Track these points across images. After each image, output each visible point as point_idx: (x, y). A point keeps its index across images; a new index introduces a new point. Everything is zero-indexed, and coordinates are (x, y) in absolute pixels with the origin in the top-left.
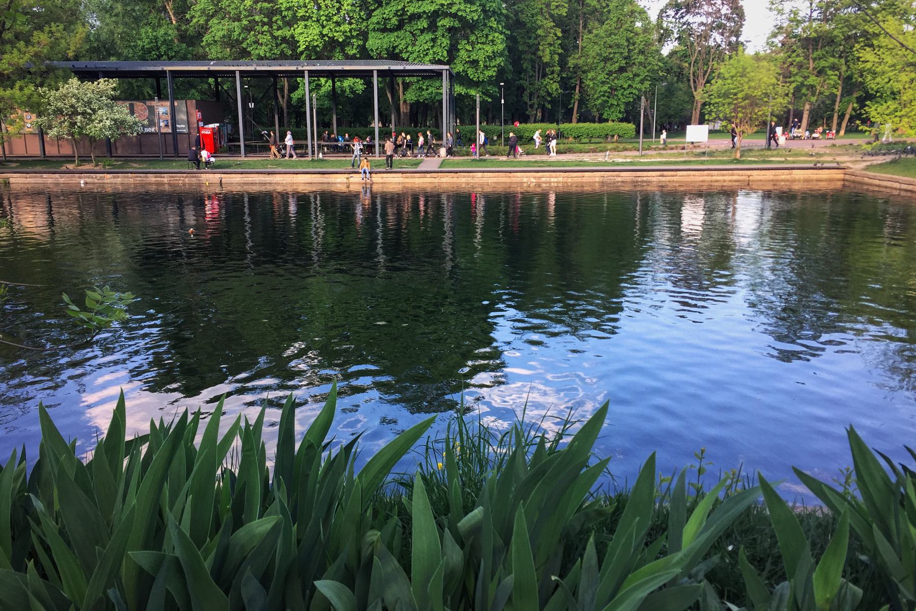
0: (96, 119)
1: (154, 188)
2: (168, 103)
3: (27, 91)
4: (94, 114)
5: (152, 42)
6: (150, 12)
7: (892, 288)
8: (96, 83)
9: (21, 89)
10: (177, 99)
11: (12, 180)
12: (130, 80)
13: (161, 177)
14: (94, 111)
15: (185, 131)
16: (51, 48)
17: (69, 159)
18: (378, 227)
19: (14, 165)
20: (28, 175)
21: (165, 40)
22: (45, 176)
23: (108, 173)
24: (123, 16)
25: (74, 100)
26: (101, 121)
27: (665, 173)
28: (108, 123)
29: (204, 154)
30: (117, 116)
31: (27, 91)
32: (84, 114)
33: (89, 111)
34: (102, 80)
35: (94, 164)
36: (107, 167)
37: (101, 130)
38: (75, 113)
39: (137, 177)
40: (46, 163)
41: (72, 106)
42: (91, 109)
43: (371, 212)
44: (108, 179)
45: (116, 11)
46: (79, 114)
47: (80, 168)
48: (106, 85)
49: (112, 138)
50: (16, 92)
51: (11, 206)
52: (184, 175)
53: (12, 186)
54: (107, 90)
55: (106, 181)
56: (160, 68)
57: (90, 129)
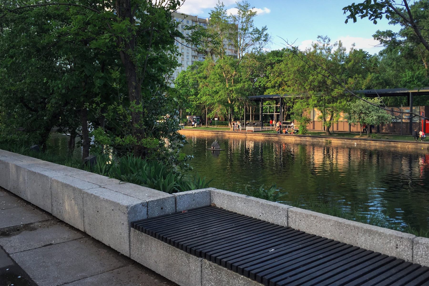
0: (370, 116)
1: (392, 149)
2: (409, 108)
3: (343, 104)
4: (370, 113)
5: (411, 78)
6: (414, 63)
7: (29, 118)
8: (373, 99)
9: (340, 103)
10: (414, 106)
11: (332, 141)
12: (397, 97)
13: (397, 144)
14: (370, 112)
15: (418, 121)
16: (356, 85)
17: (358, 133)
18: (145, 135)
19: (336, 135)
20: (339, 140)
21: (418, 77)
22: (345, 140)
23: (373, 140)
24: (396, 67)
25: (361, 107)
26: (372, 117)
27: (230, 133)
28: (375, 117)
29: (421, 133)
30: (380, 114)
31: (343, 104)
32: (365, 113)
33: (367, 112)
34: (376, 98)
35: (368, 136)
36: (374, 138)
37: (371, 120)
38: (362, 113)
39: (385, 143)
40: (349, 135)
41: (361, 110)
42: (369, 111)
43: (262, 144)
44: (373, 143)
45: (393, 65)
46: (363, 113)
47: (361, 137)
48: (377, 100)
49: (376, 125)
50: (338, 104)
51: (333, 153)
52: (409, 143)
53: (332, 143)
54: (377, 102)
55: (371, 144)
56: (406, 91)
57: (367, 120)
